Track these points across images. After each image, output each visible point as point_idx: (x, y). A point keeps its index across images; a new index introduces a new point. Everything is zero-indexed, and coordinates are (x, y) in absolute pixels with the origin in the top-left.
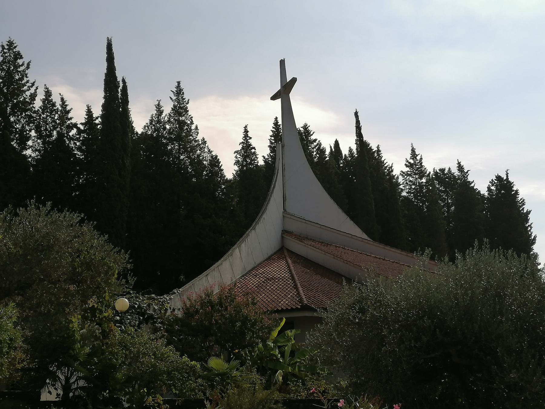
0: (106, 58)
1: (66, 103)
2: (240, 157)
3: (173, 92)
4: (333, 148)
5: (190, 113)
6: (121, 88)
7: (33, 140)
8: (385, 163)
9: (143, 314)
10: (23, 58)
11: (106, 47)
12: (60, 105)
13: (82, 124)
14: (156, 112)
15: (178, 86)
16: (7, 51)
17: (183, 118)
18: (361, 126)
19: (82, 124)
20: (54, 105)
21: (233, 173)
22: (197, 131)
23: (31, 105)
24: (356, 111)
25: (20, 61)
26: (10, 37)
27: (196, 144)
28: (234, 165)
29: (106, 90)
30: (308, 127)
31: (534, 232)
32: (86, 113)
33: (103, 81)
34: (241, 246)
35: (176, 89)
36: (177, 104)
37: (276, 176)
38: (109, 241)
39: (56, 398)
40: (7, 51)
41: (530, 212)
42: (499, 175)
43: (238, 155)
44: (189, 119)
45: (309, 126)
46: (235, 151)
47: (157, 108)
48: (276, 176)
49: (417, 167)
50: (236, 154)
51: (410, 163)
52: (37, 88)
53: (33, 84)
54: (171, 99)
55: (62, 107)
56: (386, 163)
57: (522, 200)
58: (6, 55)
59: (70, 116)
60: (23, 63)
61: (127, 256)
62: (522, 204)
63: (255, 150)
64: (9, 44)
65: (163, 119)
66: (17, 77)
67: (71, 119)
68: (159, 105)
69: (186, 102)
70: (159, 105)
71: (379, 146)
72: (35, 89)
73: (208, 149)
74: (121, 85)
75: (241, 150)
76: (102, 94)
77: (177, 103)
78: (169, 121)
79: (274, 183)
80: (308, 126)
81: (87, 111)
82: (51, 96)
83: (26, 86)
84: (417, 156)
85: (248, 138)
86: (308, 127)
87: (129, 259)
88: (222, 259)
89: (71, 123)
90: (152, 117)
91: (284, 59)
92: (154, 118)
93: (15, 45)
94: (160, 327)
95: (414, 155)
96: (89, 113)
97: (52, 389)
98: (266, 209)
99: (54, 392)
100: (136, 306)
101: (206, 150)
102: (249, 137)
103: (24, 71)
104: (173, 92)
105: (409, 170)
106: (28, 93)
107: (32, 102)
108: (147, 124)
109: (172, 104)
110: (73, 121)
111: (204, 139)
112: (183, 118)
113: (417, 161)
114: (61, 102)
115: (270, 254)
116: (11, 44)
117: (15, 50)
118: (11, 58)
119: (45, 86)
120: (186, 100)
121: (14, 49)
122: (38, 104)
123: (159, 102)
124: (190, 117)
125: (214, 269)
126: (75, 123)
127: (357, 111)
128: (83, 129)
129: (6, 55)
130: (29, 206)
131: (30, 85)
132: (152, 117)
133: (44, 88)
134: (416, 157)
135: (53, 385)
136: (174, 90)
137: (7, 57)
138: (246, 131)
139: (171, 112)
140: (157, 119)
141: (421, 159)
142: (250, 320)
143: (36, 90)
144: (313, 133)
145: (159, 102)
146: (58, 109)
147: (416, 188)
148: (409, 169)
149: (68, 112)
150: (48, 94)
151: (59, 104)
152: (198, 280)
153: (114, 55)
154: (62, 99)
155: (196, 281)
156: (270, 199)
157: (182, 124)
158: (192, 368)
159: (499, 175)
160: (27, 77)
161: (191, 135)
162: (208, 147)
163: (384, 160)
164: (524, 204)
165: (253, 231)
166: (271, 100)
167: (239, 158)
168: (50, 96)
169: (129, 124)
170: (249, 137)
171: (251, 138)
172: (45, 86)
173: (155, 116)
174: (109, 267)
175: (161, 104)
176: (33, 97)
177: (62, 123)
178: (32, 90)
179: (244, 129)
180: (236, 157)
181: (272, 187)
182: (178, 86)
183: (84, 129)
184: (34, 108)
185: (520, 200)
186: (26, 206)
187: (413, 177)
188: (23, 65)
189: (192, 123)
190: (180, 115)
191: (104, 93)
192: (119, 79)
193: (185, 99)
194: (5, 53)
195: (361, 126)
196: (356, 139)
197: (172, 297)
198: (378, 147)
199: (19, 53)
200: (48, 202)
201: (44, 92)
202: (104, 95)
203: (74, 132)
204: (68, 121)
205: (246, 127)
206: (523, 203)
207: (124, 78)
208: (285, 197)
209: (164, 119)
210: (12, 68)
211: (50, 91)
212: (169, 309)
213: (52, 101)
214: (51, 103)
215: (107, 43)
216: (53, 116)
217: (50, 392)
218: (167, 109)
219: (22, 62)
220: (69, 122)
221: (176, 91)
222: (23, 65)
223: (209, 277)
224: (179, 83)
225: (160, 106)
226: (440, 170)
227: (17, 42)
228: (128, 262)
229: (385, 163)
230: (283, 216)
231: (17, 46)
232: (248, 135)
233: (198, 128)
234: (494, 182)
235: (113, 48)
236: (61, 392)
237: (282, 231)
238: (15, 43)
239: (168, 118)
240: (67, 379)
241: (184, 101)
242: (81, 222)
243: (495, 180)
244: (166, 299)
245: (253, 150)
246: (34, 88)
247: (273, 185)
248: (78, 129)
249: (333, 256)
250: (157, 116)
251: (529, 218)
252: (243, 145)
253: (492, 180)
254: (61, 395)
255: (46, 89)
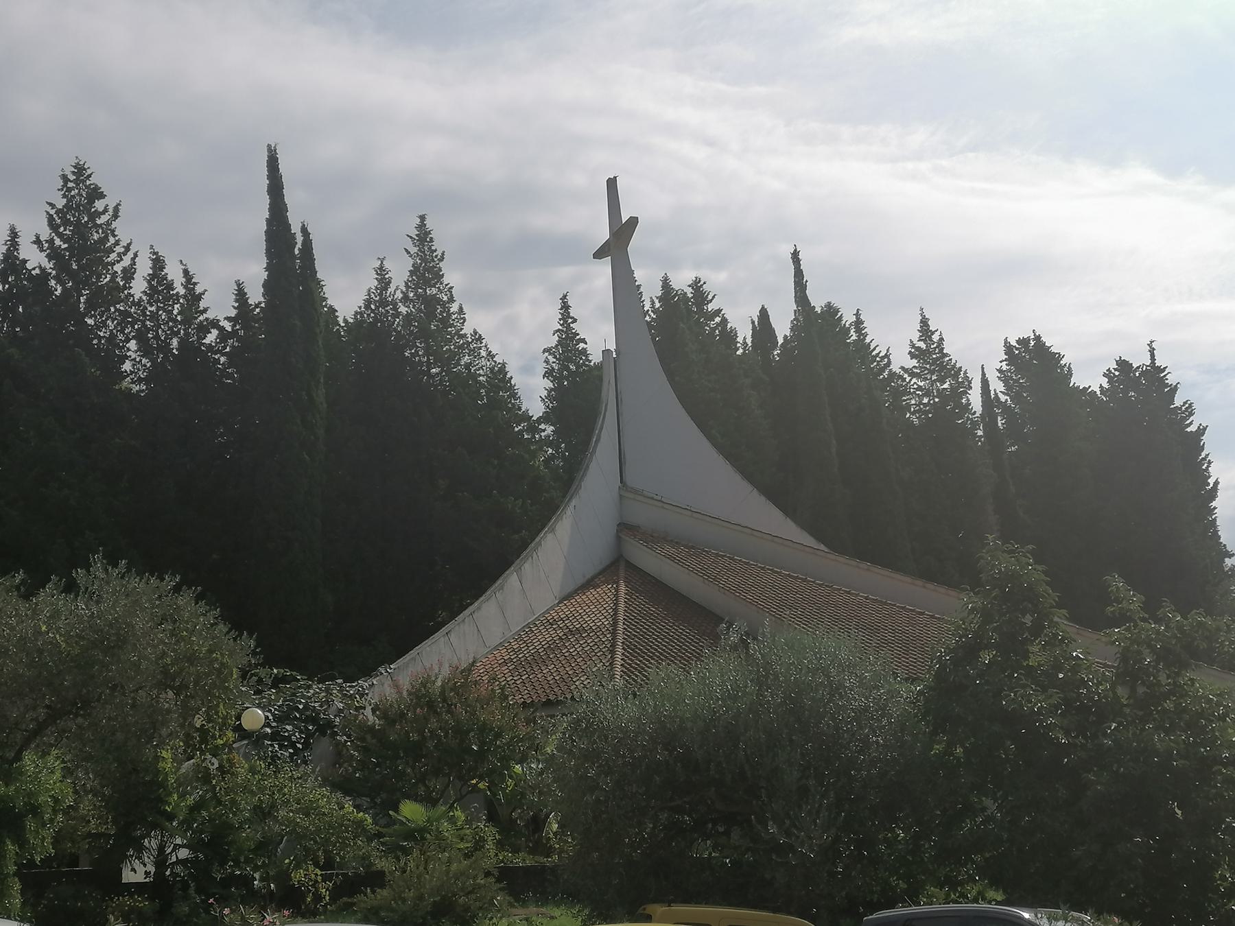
0: (266, 188)
1: (193, 280)
2: (555, 360)
3: (411, 237)
4: (756, 323)
5: (446, 280)
6: (299, 245)
7: (132, 360)
8: (872, 348)
9: (314, 720)
10: (106, 196)
11: (266, 164)
12: (182, 284)
13: (228, 319)
14: (376, 283)
15: (422, 226)
16: (74, 186)
17: (434, 291)
18: (807, 281)
19: (228, 319)
20: (170, 286)
21: (541, 397)
22: (462, 316)
23: (126, 292)
24: (796, 250)
25: (99, 205)
26: (77, 157)
27: (461, 342)
28: (544, 378)
29: (269, 253)
30: (702, 285)
31: (1217, 472)
32: (235, 297)
33: (264, 233)
34: (522, 568)
35: (418, 231)
36: (419, 262)
37: (602, 417)
38: (224, 617)
39: (145, 878)
40: (74, 186)
41: (1205, 429)
42: (1122, 359)
43: (550, 357)
44: (446, 292)
45: (705, 283)
46: (544, 349)
47: (377, 274)
48: (602, 417)
49: (934, 356)
50: (547, 354)
51: (918, 349)
52: (136, 255)
53: (127, 248)
54: (408, 252)
55: (185, 287)
56: (876, 347)
57: (1187, 405)
58: (73, 193)
59: (202, 305)
60: (105, 207)
61: (252, 643)
62: (1187, 413)
63: (586, 343)
64: (76, 171)
65: (392, 296)
66: (96, 237)
67: (205, 310)
68: (381, 268)
69: (439, 257)
70: (381, 268)
71: (860, 312)
72: (133, 256)
73: (487, 350)
74: (299, 239)
75: (557, 346)
76: (264, 262)
77: (420, 259)
78: (405, 299)
79: (597, 432)
80: (702, 283)
81: (236, 292)
82: (165, 268)
83: (114, 252)
84: (933, 333)
85: (570, 320)
86: (702, 285)
87: (256, 647)
88: (481, 599)
89: (207, 319)
90: (369, 295)
91: (615, 177)
92: (373, 296)
93: (89, 172)
94: (346, 741)
95: (925, 330)
96: (241, 295)
97: (137, 863)
98: (579, 487)
99: (141, 870)
100: (301, 707)
101: (483, 353)
102: (571, 318)
103: (108, 223)
104: (411, 237)
105: (917, 365)
106: (118, 268)
107: (127, 285)
108: (360, 308)
109: (411, 262)
110: (210, 315)
111: (475, 332)
112: (434, 291)
113: (933, 344)
114: (183, 277)
115: (591, 575)
116: (80, 170)
117: (88, 183)
118: (83, 199)
119: (150, 249)
120: (439, 253)
121: (88, 181)
122: (138, 287)
123: (382, 262)
124: (448, 286)
125: (463, 621)
126: (214, 319)
127: (798, 250)
128: (230, 330)
129: (73, 193)
130: (92, 566)
131: (119, 249)
132: (369, 295)
133: (151, 253)
134: (930, 337)
135: (139, 858)
136: (414, 233)
137: (73, 197)
138: (565, 307)
139: (408, 280)
140: (378, 297)
141: (942, 339)
142: (492, 729)
143: (133, 259)
144: (714, 297)
145: (382, 262)
146: (178, 293)
147: (931, 402)
148: (916, 361)
149: (199, 297)
150: (158, 263)
151: (180, 283)
152: (429, 644)
153: (283, 180)
154: (186, 272)
155: (425, 646)
156: (588, 466)
157: (431, 303)
158: (360, 824)
159: (1122, 359)
160: (114, 236)
161: (452, 326)
162: (486, 346)
163: (871, 342)
164: (1191, 414)
165: (550, 536)
166: (637, 218)
167: (554, 362)
168: (162, 268)
169: (318, 317)
170: (571, 318)
171: (575, 321)
172: (150, 249)
173: (375, 291)
174: (222, 664)
175: (387, 265)
176: (129, 274)
177: (187, 321)
178: (126, 261)
179: (561, 301)
180: (547, 362)
181: (594, 439)
182: (422, 226)
183: (232, 329)
184: (133, 296)
185: (1183, 406)
186: (87, 567)
187: (926, 379)
188: (105, 211)
189: (452, 300)
190: (428, 283)
191: (266, 258)
192: (296, 229)
193: (436, 251)
194: (69, 190)
195: (807, 281)
196: (795, 308)
197: (375, 682)
198: (857, 314)
199: (97, 188)
200: (121, 561)
201: (151, 262)
202: (267, 263)
203: (211, 337)
204: (199, 316)
205: (565, 296)
206: (1189, 410)
207: (304, 225)
208: (624, 458)
209: (394, 296)
210: (86, 219)
211: (161, 258)
212: (367, 705)
213: (166, 279)
214: (165, 282)
215: (268, 156)
216: (170, 308)
217: (133, 870)
218: (400, 273)
219: (104, 206)
220: (201, 318)
221: (417, 235)
222: (105, 211)
223: (453, 637)
224: (422, 218)
225: (384, 271)
226: (1018, 342)
227: (92, 166)
228: (254, 653)
229: (872, 348)
230: (621, 495)
231: (92, 174)
232: (569, 313)
233: (465, 310)
234: (1114, 374)
235: (279, 167)
236: (151, 869)
237: (618, 525)
238: (89, 168)
239: (402, 292)
240: (161, 848)
241: (434, 255)
242: (177, 589)
243: (1115, 369)
244: (362, 687)
245: (582, 345)
246: (130, 254)
247: (595, 437)
248: (221, 329)
249: (701, 578)
250: (378, 291)
251: (1202, 443)
252: (560, 335)
253: (1109, 370)
254: (152, 873)
255: (153, 255)
